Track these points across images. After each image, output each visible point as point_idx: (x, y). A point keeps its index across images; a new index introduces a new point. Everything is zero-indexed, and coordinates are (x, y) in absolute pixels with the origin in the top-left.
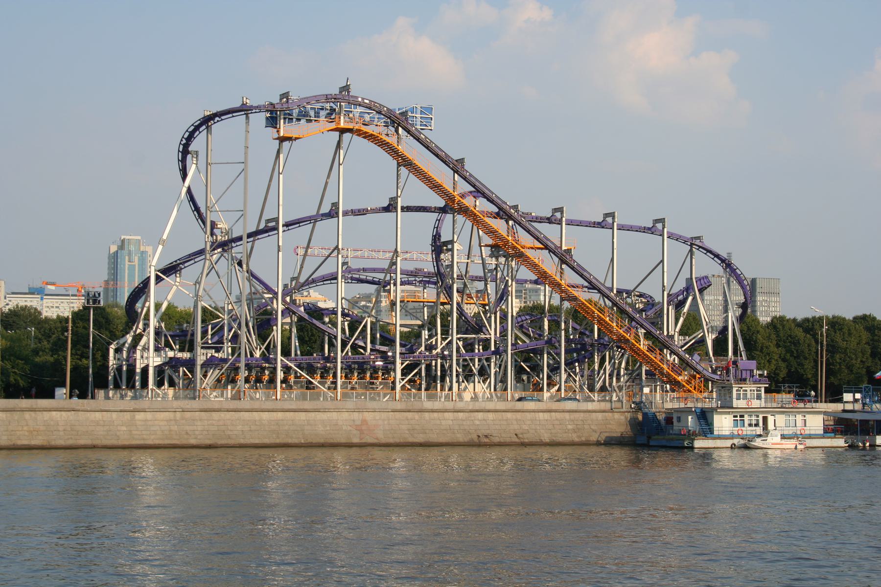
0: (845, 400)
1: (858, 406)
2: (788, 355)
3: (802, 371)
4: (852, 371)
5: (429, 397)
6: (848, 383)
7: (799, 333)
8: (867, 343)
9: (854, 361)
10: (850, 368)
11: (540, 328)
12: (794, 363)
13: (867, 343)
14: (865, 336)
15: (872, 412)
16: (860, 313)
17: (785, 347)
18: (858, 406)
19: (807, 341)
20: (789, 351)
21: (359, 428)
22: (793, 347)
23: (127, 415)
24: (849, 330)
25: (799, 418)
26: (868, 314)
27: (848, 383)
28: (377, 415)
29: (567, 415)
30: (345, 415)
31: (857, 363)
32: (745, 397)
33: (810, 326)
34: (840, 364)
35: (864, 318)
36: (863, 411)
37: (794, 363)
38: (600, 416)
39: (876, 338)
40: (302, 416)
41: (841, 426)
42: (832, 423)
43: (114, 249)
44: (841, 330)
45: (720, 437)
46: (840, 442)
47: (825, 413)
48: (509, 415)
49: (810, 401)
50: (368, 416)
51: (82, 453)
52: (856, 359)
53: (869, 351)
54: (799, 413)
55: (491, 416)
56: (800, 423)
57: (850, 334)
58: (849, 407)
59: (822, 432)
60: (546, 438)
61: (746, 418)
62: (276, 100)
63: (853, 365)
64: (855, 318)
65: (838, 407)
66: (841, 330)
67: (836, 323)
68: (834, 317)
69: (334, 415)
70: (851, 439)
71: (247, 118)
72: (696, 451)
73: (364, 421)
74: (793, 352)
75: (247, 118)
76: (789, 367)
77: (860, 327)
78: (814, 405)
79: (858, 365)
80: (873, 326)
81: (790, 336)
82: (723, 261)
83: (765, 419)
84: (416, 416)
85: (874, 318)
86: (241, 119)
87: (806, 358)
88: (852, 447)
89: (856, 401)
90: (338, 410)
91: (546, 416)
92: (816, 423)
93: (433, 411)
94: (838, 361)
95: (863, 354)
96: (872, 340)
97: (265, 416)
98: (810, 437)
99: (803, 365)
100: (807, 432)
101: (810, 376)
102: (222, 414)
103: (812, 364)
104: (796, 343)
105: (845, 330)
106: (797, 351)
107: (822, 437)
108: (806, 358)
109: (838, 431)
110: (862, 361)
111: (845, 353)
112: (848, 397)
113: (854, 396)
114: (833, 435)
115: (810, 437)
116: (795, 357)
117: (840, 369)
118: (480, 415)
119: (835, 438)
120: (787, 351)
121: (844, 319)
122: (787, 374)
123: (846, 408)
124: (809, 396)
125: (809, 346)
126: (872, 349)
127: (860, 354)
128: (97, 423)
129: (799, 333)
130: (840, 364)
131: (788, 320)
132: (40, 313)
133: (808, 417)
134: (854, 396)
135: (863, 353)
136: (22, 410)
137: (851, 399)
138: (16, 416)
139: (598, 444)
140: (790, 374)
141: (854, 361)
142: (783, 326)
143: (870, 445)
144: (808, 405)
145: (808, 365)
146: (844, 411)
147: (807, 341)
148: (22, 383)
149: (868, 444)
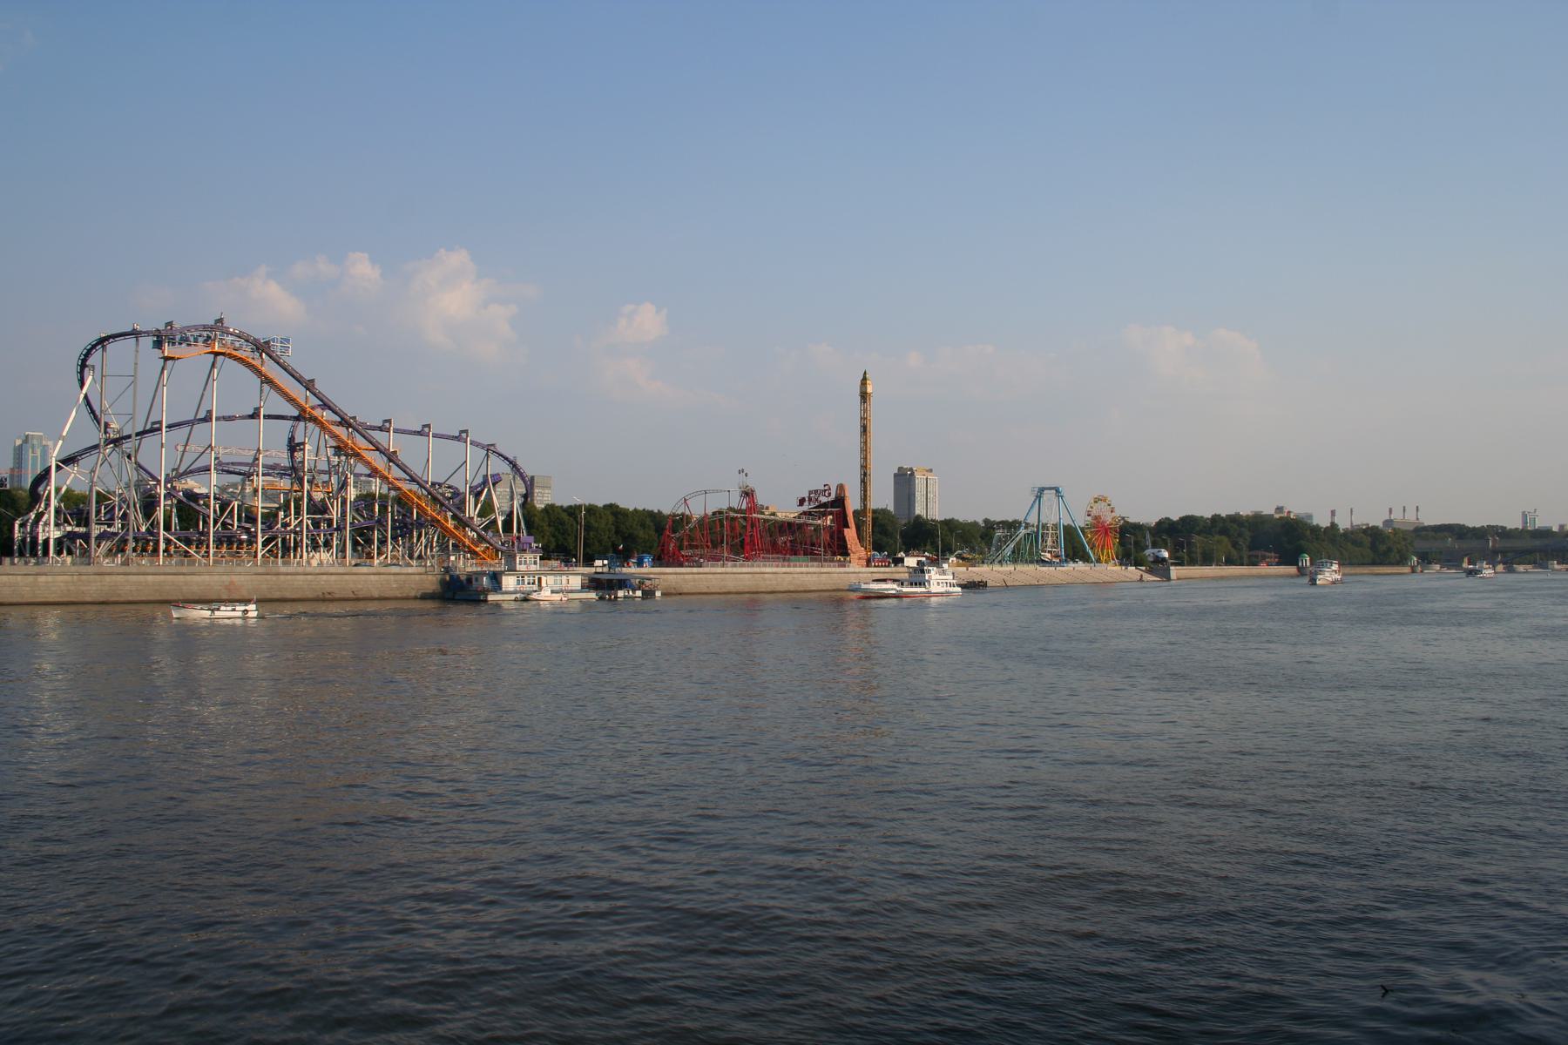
1: (606, 570)
5: (284, 564)
7: (565, 516)
14: (611, 518)
21: (227, 588)
23: (31, 578)
28: (242, 578)
30: (216, 578)
33: (572, 511)
35: (611, 506)
41: (594, 583)
46: (593, 595)
65: (593, 570)
67: (591, 510)
69: (207, 578)
73: (232, 583)
88: (601, 598)
92: (576, 582)
104: (562, 523)
112: (598, 563)
129: (565, 516)
139: (415, 598)
145: (571, 540)
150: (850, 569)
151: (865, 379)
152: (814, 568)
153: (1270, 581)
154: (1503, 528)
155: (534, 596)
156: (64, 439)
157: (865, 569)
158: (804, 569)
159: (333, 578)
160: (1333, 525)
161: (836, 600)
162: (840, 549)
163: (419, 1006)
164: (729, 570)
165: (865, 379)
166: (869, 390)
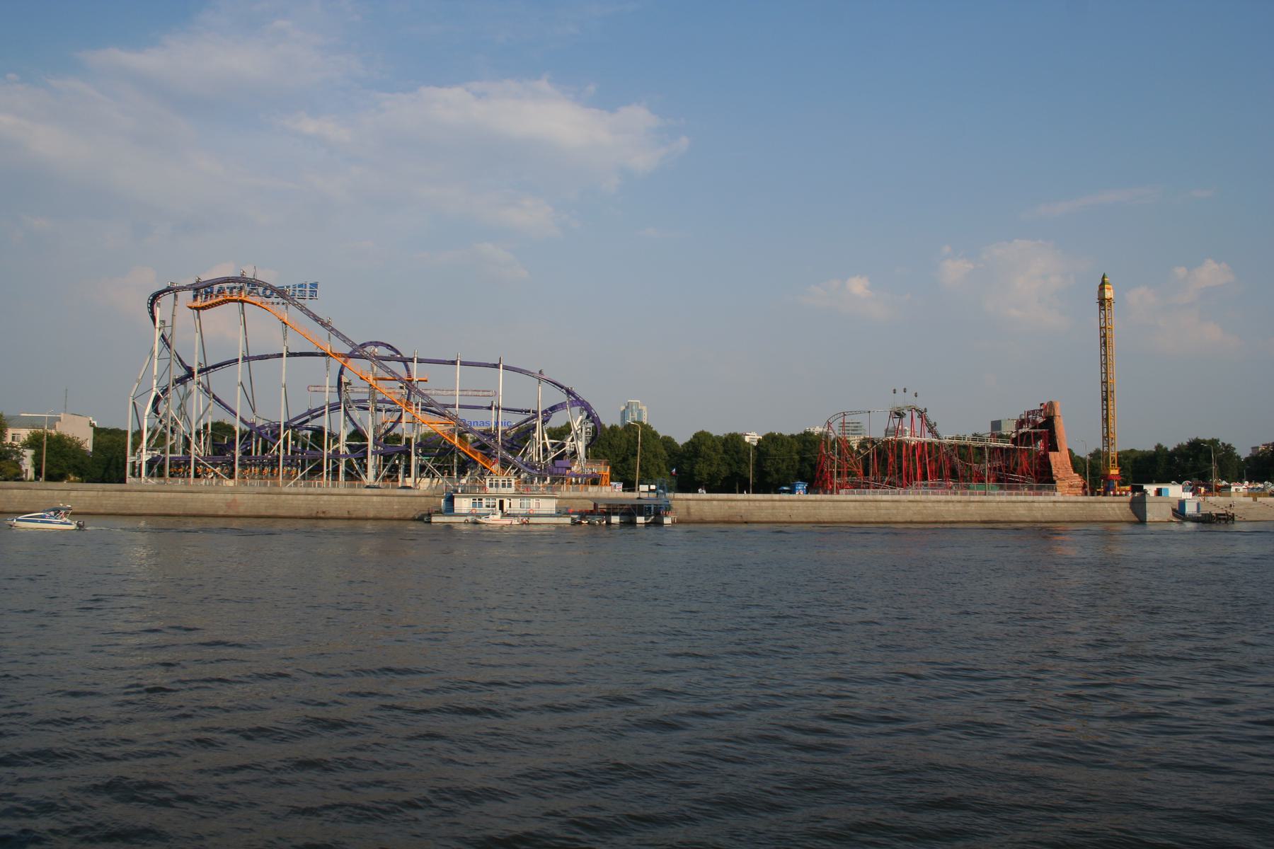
5: (334, 486)
21: (229, 506)
23: (65, 493)
28: (245, 496)
29: (396, 499)
30: (222, 496)
32: (497, 485)
43: (623, 408)
51: (206, 520)
58: (644, 495)
60: (371, 515)
61: (484, 501)
69: (213, 496)
71: (176, 296)
72: (1151, 528)
73: (234, 500)
75: (176, 296)
83: (501, 503)
84: (275, 497)
86: (170, 296)
89: (650, 491)
91: (379, 499)
92: (549, 506)
112: (644, 488)
118: (325, 498)
128: (43, 498)
139: (414, 519)
150: (1058, 496)
151: (1103, 283)
152: (856, 496)
153: (236, 524)
154: (733, 443)
155: (483, 520)
156: (138, 381)
157: (1081, 498)
158: (943, 498)
159: (334, 498)
160: (827, 436)
161: (1044, 531)
162: (1044, 477)
163: (1166, 842)
164: (870, 497)
165: (1103, 283)
166: (1109, 294)
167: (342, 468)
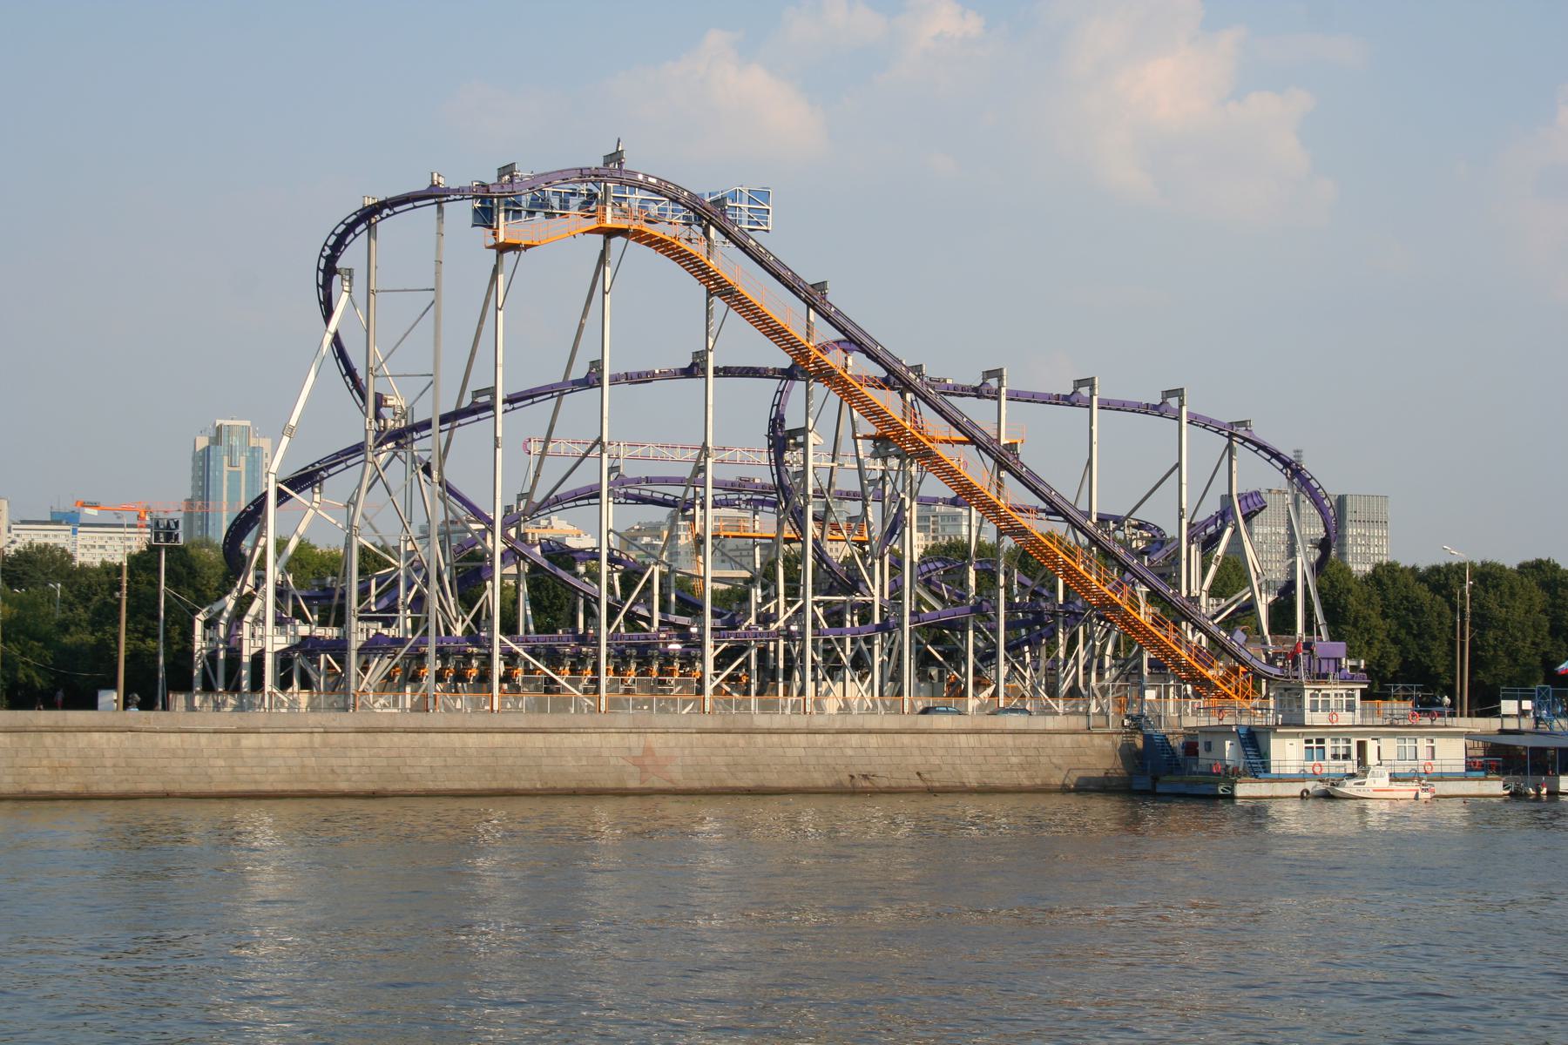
0: (1503, 712)
1: (1527, 724)
2: (1403, 631)
3: (1427, 661)
4: (1516, 660)
5: (764, 708)
6: (1510, 682)
7: (1423, 593)
8: (1544, 611)
9: (1520, 644)
10: (1512, 655)
11: (961, 584)
12: (1413, 646)
13: (1544, 611)
14: (1540, 597)
15: (1551, 734)
16: (1530, 558)
17: (1397, 617)
18: (1527, 724)
19: (1436, 608)
20: (1404, 624)
21: (639, 763)
22: (1411, 617)
23: (227, 740)
24: (1512, 587)
25: (1423, 743)
26: (1545, 558)
27: (1510, 682)
28: (671, 739)
29: (1009, 740)
30: (615, 739)
31: (1525, 646)
32: (1326, 707)
33: (1441, 580)
34: (1495, 647)
35: (1538, 566)
36: (1535, 732)
37: (1413, 646)
38: (1068, 740)
39: (1559, 601)
40: (538, 740)
41: (1496, 758)
42: (1480, 753)
43: (202, 442)
44: (1496, 587)
45: (1281, 779)
46: (1495, 787)
47: (1468, 735)
48: (906, 739)
49: (1441, 714)
50: (656, 741)
51: (145, 806)
52: (1524, 640)
53: (1546, 624)
54: (1422, 735)
55: (873, 740)
56: (1423, 753)
57: (1513, 595)
58: (1511, 724)
59: (1463, 769)
60: (972, 780)
61: (1328, 744)
62: (491, 178)
63: (1518, 650)
64: (1521, 566)
65: (1491, 724)
66: (1496, 587)
67: (1488, 576)
68: (1484, 565)
69: (595, 739)
70: (1515, 781)
71: (440, 210)
72: (1239, 802)
73: (648, 750)
74: (1411, 627)
75: (440, 210)
76: (1403, 653)
77: (1531, 583)
78: (1449, 720)
79: (1527, 651)
80: (1554, 580)
81: (1406, 598)
82: (1287, 464)
83: (1362, 746)
84: (741, 740)
85: (1556, 567)
86: (428, 211)
87: (1434, 638)
88: (1517, 795)
89: (1523, 713)
90: (602, 730)
91: (972, 740)
92: (1452, 753)
93: (770, 732)
94: (1492, 642)
95: (1536, 630)
96: (1553, 605)
97: (472, 740)
98: (1442, 777)
99: (1428, 650)
100: (1437, 769)
101: (1441, 670)
102: (396, 738)
103: (1446, 648)
104: (1417, 610)
105: (1505, 588)
106: (1419, 624)
107: (1463, 778)
108: (1434, 638)
109: (1491, 767)
110: (1533, 643)
111: (1504, 628)
112: (1509, 706)
113: (1520, 705)
114: (1482, 774)
115: (1442, 777)
116: (1415, 636)
117: (1495, 656)
118: (854, 739)
119: (1486, 779)
120: (1401, 626)
121: (1502, 568)
122: (1401, 665)
123: (1506, 727)
124: (1441, 704)
125: (1439, 615)
126: (1551, 621)
127: (1531, 631)
128: (173, 754)
129: (1423, 593)
130: (1495, 647)
131: (1402, 570)
132: (71, 557)
133: (1438, 742)
134: (1520, 705)
135: (1536, 629)
136: (40, 731)
137: (1515, 711)
138: (29, 740)
139: (1064, 790)
140: (1405, 666)
141: (1520, 644)
142: (1394, 581)
143: (1548, 793)
144: (1439, 721)
145: (1438, 650)
146: (1503, 732)
147: (1436, 608)
148: (39, 682)
149: (1544, 791)
167: (498, 668)
